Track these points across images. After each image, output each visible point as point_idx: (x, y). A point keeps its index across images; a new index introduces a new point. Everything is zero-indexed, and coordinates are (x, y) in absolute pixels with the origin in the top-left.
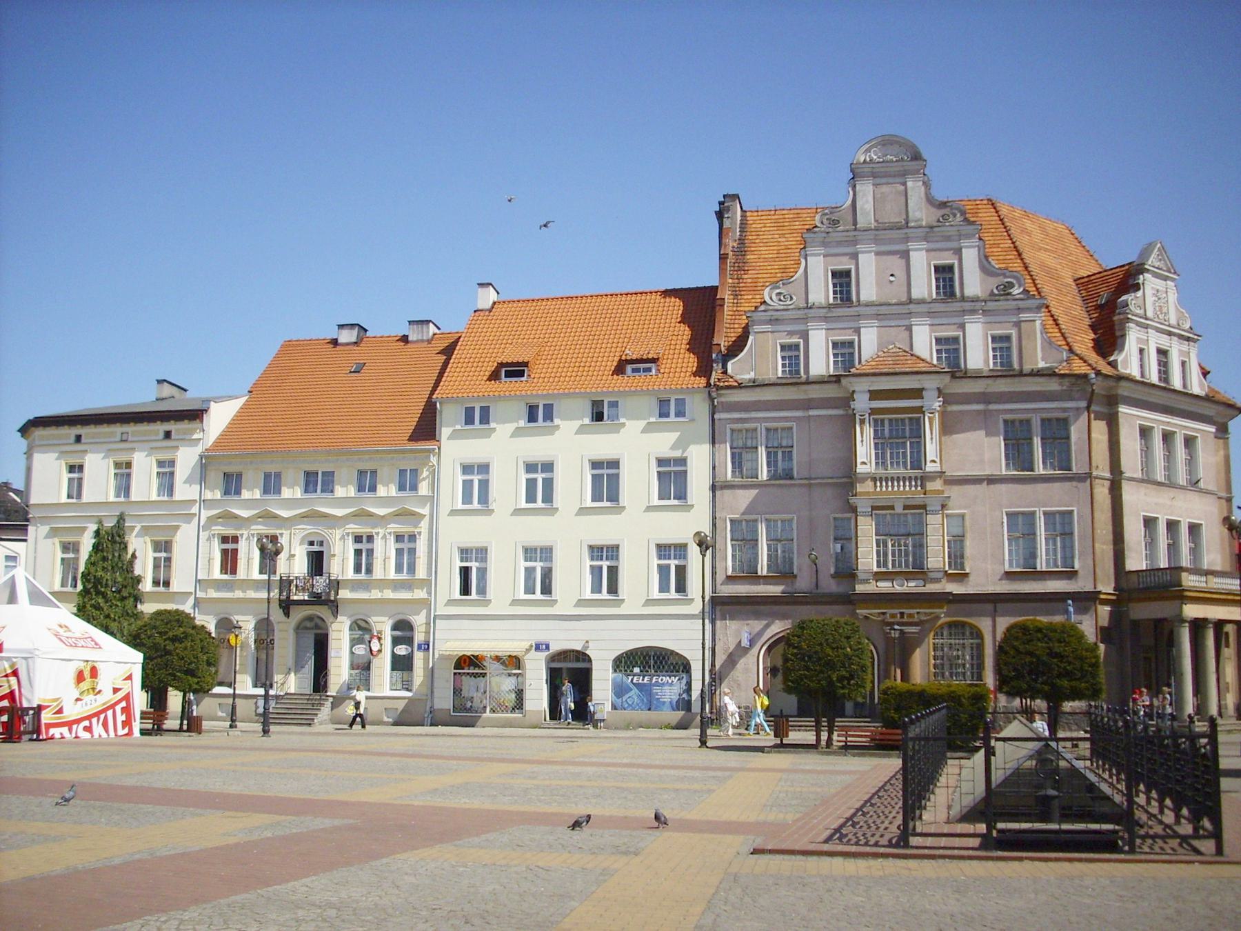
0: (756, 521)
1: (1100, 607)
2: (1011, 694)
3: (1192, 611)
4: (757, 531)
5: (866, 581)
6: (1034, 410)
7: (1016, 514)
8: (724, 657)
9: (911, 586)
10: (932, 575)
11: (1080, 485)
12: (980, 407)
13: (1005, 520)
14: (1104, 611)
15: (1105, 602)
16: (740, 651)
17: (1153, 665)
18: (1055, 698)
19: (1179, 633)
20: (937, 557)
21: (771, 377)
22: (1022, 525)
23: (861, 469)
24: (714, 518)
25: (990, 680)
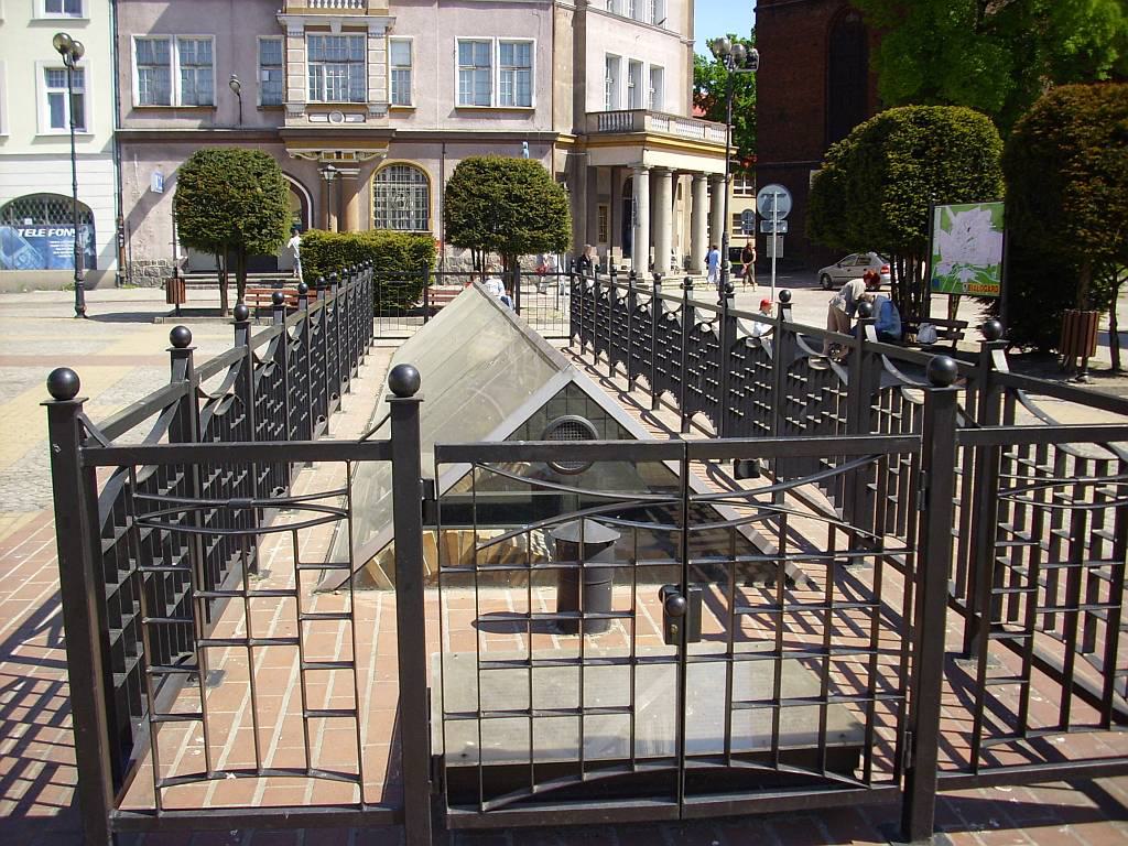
0: (166, 42)
1: (557, 151)
2: (460, 245)
3: (653, 158)
4: (168, 53)
5: (298, 115)
7: (470, 43)
8: (133, 204)
9: (350, 122)
10: (373, 109)
11: (542, 13)
13: (457, 49)
14: (561, 155)
15: (562, 146)
16: (152, 198)
17: (609, 214)
18: (510, 251)
19: (638, 180)
20: (379, 89)
22: (475, 55)
24: (116, 36)
25: (436, 228)
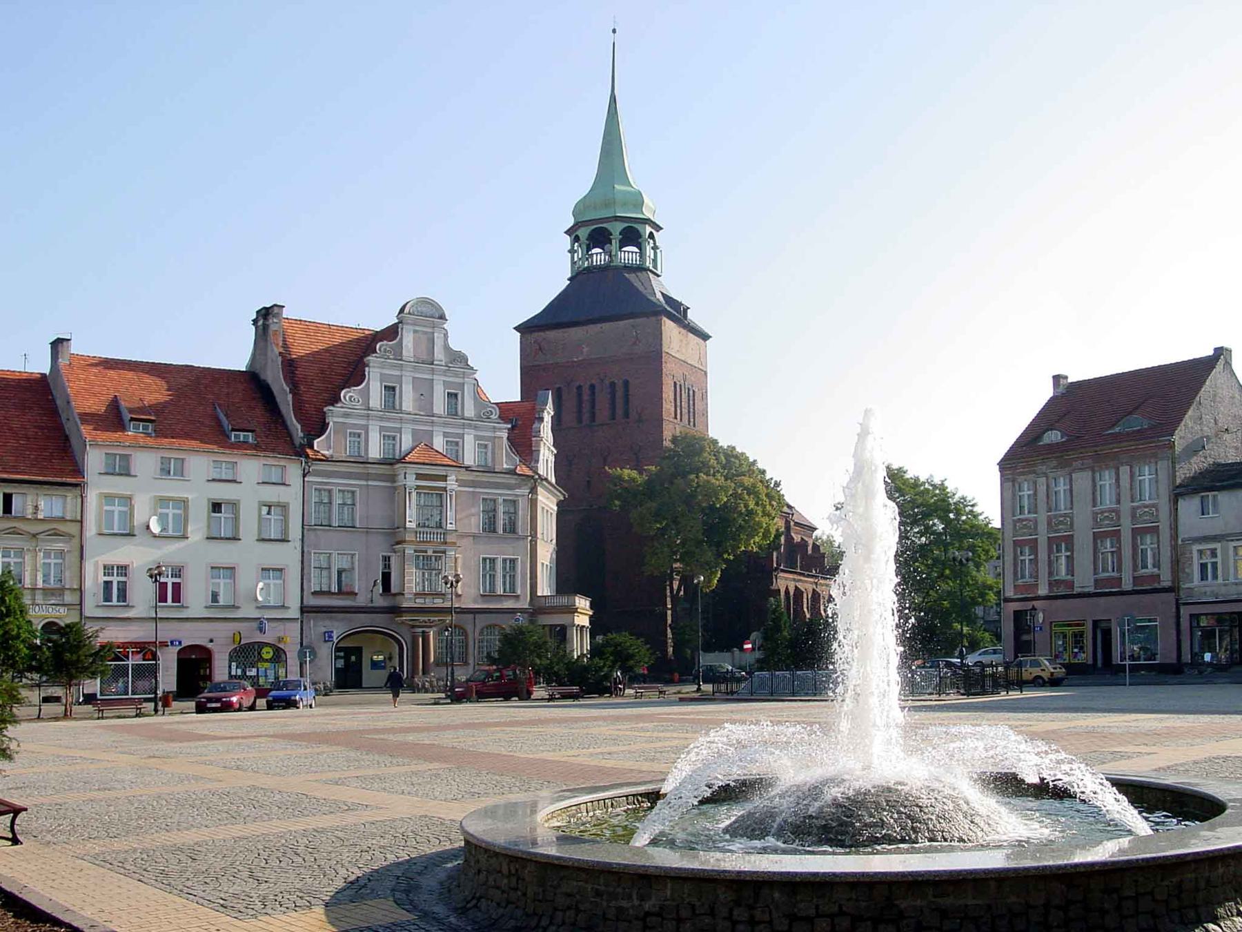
6: (500, 495)
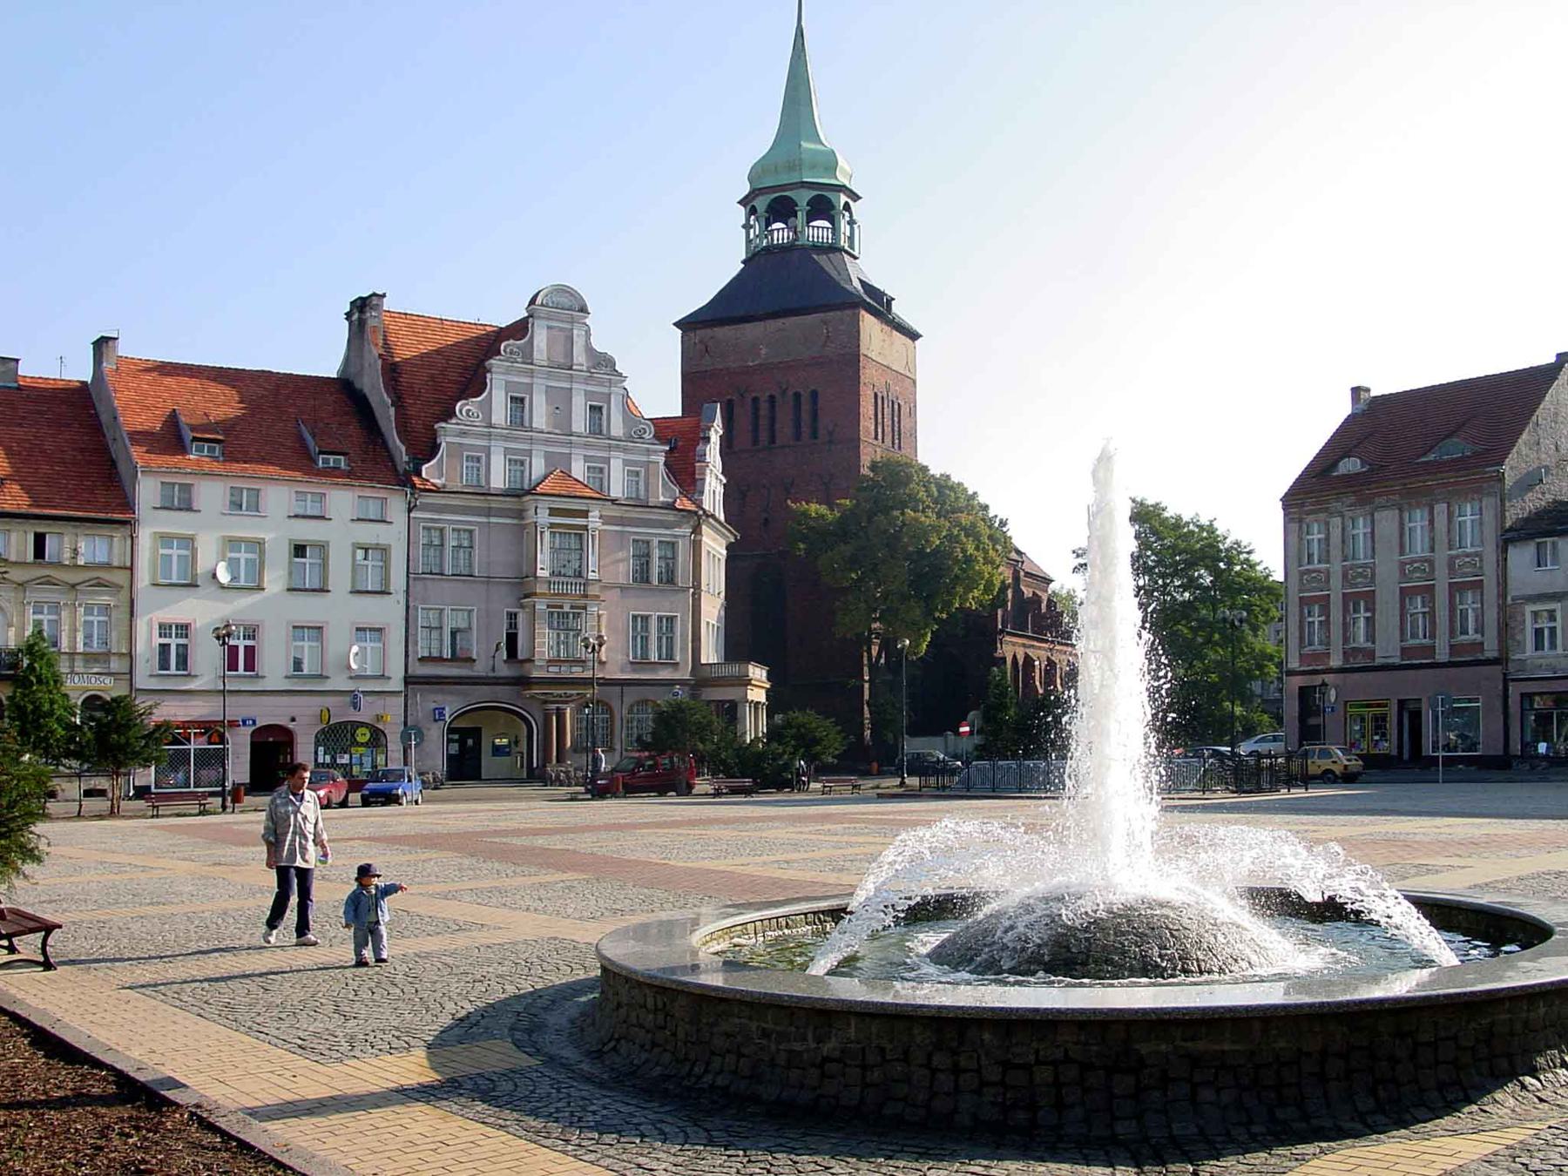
12: (484, 520)
21: (457, 487)
23: (540, 573)
